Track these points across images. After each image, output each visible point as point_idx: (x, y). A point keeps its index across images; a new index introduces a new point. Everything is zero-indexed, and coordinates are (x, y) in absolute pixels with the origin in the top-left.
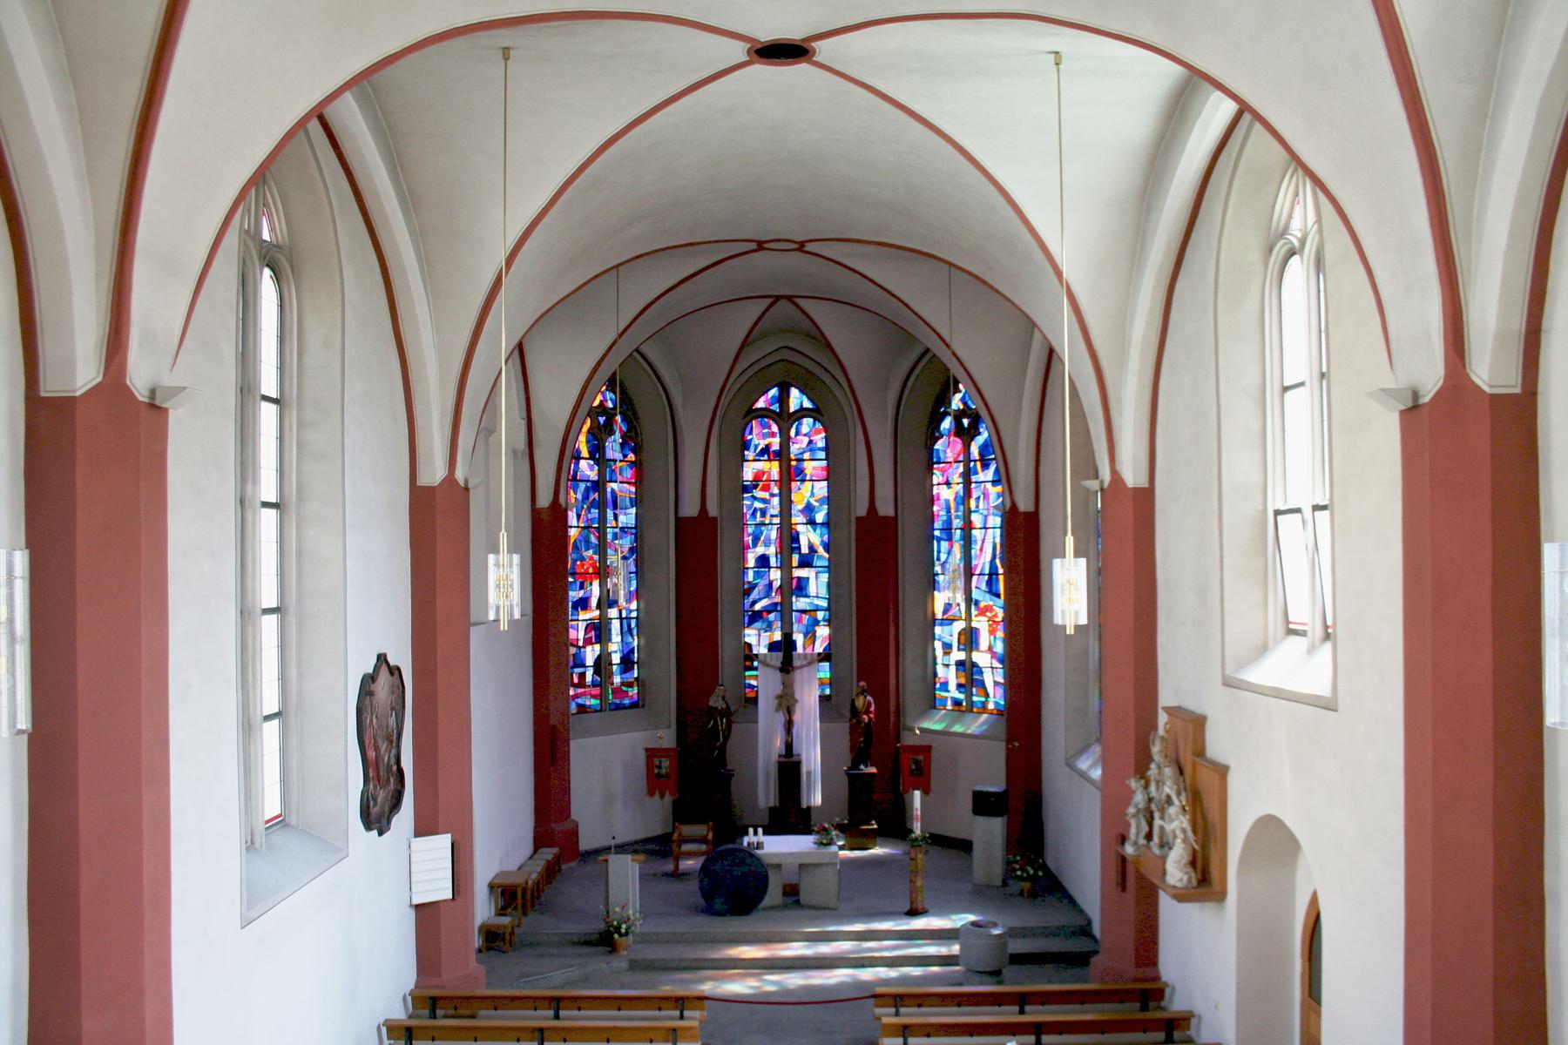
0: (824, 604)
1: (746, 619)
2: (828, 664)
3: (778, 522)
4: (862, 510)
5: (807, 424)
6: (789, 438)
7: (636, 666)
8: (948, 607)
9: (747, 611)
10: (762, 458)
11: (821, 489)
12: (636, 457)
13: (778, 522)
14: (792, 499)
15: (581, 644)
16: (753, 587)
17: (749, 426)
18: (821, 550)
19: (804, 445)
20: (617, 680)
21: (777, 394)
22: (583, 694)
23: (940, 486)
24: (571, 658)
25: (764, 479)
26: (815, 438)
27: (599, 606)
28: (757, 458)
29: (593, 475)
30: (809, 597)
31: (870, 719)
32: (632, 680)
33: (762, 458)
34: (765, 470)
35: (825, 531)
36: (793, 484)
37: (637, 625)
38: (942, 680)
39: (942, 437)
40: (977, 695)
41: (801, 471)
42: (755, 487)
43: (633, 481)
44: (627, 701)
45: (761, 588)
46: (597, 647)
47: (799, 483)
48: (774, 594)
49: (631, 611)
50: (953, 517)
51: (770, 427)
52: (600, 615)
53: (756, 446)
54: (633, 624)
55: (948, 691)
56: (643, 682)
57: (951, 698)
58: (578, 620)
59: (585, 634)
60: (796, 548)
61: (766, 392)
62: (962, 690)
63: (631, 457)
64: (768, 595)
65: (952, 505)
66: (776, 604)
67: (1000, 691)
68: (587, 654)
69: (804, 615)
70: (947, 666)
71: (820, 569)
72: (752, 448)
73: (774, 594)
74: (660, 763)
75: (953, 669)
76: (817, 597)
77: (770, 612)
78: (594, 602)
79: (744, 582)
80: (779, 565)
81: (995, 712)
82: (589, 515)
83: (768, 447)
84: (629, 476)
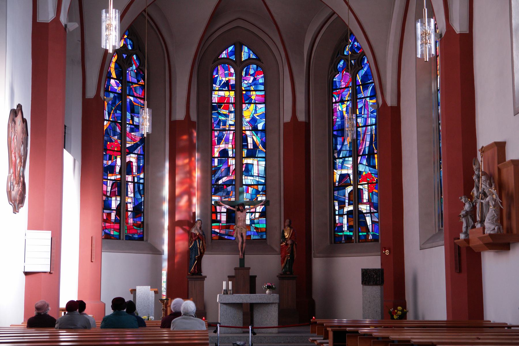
1: (213, 189)
2: (265, 219)
4: (287, 118)
6: (242, 76)
8: (342, 176)
9: (214, 185)
10: (224, 89)
11: (261, 108)
15: (109, 194)
16: (218, 169)
18: (261, 147)
19: (251, 81)
20: (131, 221)
21: (234, 50)
22: (110, 227)
28: (221, 89)
30: (253, 176)
33: (224, 89)
36: (244, 105)
38: (338, 225)
41: (249, 97)
42: (220, 107)
47: (247, 105)
53: (221, 81)
64: (227, 175)
69: (250, 188)
72: (218, 83)
78: (118, 169)
79: (212, 166)
80: (234, 156)
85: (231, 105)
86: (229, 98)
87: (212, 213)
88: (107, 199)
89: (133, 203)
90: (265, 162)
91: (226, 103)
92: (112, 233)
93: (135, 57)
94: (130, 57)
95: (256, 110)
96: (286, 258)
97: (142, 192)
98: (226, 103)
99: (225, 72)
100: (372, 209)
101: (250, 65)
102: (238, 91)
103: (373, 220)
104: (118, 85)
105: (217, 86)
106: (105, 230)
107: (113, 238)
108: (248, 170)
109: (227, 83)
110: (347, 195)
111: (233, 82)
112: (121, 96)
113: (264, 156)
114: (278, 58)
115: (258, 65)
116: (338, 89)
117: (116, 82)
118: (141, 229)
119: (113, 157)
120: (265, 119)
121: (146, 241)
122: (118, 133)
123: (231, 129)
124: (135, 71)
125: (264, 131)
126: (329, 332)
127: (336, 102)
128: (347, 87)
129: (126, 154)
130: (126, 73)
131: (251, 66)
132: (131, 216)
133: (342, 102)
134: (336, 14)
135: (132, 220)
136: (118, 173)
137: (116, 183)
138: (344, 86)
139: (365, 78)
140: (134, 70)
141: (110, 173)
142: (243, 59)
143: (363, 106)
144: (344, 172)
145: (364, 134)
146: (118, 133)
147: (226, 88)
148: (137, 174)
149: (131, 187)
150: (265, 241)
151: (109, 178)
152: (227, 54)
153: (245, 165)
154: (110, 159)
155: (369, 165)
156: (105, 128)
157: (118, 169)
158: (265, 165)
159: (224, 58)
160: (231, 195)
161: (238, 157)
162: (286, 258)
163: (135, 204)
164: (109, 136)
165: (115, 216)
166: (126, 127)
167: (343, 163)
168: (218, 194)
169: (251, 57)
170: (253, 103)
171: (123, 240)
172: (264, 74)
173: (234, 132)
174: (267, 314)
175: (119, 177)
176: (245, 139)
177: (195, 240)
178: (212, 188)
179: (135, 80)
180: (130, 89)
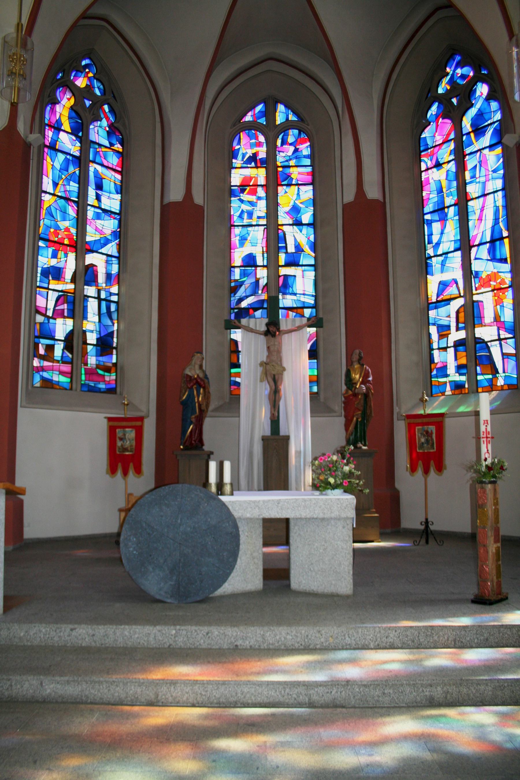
0: (311, 301)
2: (316, 361)
3: (265, 223)
4: (350, 196)
5: (292, 135)
6: (276, 146)
7: (114, 351)
8: (443, 286)
9: (234, 309)
10: (249, 166)
11: (307, 192)
12: (123, 149)
13: (265, 223)
14: (279, 202)
15: (50, 313)
16: (240, 285)
17: (237, 137)
18: (307, 249)
19: (290, 153)
20: (92, 361)
21: (264, 110)
22: (52, 369)
23: (430, 171)
24: (38, 326)
25: (251, 184)
26: (300, 147)
27: (73, 280)
28: (245, 165)
29: (75, 149)
30: (295, 294)
31: (368, 389)
32: (110, 365)
33: (249, 166)
34: (252, 176)
35: (311, 230)
36: (280, 188)
37: (117, 310)
38: (439, 366)
39: (429, 124)
40: (482, 374)
41: (288, 176)
42: (243, 191)
43: (120, 169)
44: (102, 386)
45: (247, 286)
46: (69, 323)
47: (285, 187)
48: (260, 292)
49: (111, 294)
50: (445, 195)
51: (257, 138)
52: (75, 289)
53: (244, 155)
54: (113, 307)
55: (447, 376)
56: (122, 368)
57: (450, 382)
58: (48, 288)
59: (56, 305)
60: (282, 247)
61: (254, 108)
62: (464, 371)
63: (118, 147)
64: (254, 293)
65: (444, 184)
66: (262, 301)
67: (511, 364)
68: (57, 326)
69: (290, 313)
70: (445, 349)
71: (306, 268)
72: (240, 157)
73: (260, 292)
74: (124, 435)
75: (451, 351)
76: (304, 294)
77: (256, 309)
78: (68, 274)
79: (231, 280)
80: (265, 264)
81: (506, 387)
82: (68, 187)
83: (255, 155)
84: (115, 164)
86: (256, 178)
87: (232, 352)
88: (47, 322)
89: (96, 331)
90: (314, 273)
93: (106, 107)
95: (298, 194)
96: (355, 419)
97: (115, 316)
98: (252, 186)
99: (251, 141)
100: (501, 332)
101: (289, 129)
102: (271, 167)
103: (504, 352)
105: (238, 162)
106: (41, 373)
107: (58, 387)
109: (254, 158)
110: (453, 315)
113: (313, 262)
115: (301, 129)
116: (431, 148)
118: (112, 374)
120: (314, 207)
122: (71, 218)
123: (260, 223)
124: (105, 129)
125: (312, 226)
126: (70, 278)
127: (427, 169)
128: (446, 141)
129: (84, 251)
131: (291, 132)
132: (94, 352)
133: (438, 165)
134: (290, 548)
136: (69, 281)
137: (65, 296)
138: (441, 142)
140: (105, 127)
141: (53, 279)
142: (278, 122)
143: (476, 166)
144: (447, 277)
145: (482, 210)
148: (106, 286)
149: (92, 305)
150: (316, 395)
151: (51, 287)
152: (254, 115)
153: (282, 277)
158: (315, 276)
162: (355, 419)
163: (100, 334)
165: (63, 350)
167: (443, 264)
170: (294, 185)
171: (76, 390)
172: (309, 141)
173: (265, 228)
174: (324, 545)
177: (191, 388)
178: (231, 314)
180: (96, 153)
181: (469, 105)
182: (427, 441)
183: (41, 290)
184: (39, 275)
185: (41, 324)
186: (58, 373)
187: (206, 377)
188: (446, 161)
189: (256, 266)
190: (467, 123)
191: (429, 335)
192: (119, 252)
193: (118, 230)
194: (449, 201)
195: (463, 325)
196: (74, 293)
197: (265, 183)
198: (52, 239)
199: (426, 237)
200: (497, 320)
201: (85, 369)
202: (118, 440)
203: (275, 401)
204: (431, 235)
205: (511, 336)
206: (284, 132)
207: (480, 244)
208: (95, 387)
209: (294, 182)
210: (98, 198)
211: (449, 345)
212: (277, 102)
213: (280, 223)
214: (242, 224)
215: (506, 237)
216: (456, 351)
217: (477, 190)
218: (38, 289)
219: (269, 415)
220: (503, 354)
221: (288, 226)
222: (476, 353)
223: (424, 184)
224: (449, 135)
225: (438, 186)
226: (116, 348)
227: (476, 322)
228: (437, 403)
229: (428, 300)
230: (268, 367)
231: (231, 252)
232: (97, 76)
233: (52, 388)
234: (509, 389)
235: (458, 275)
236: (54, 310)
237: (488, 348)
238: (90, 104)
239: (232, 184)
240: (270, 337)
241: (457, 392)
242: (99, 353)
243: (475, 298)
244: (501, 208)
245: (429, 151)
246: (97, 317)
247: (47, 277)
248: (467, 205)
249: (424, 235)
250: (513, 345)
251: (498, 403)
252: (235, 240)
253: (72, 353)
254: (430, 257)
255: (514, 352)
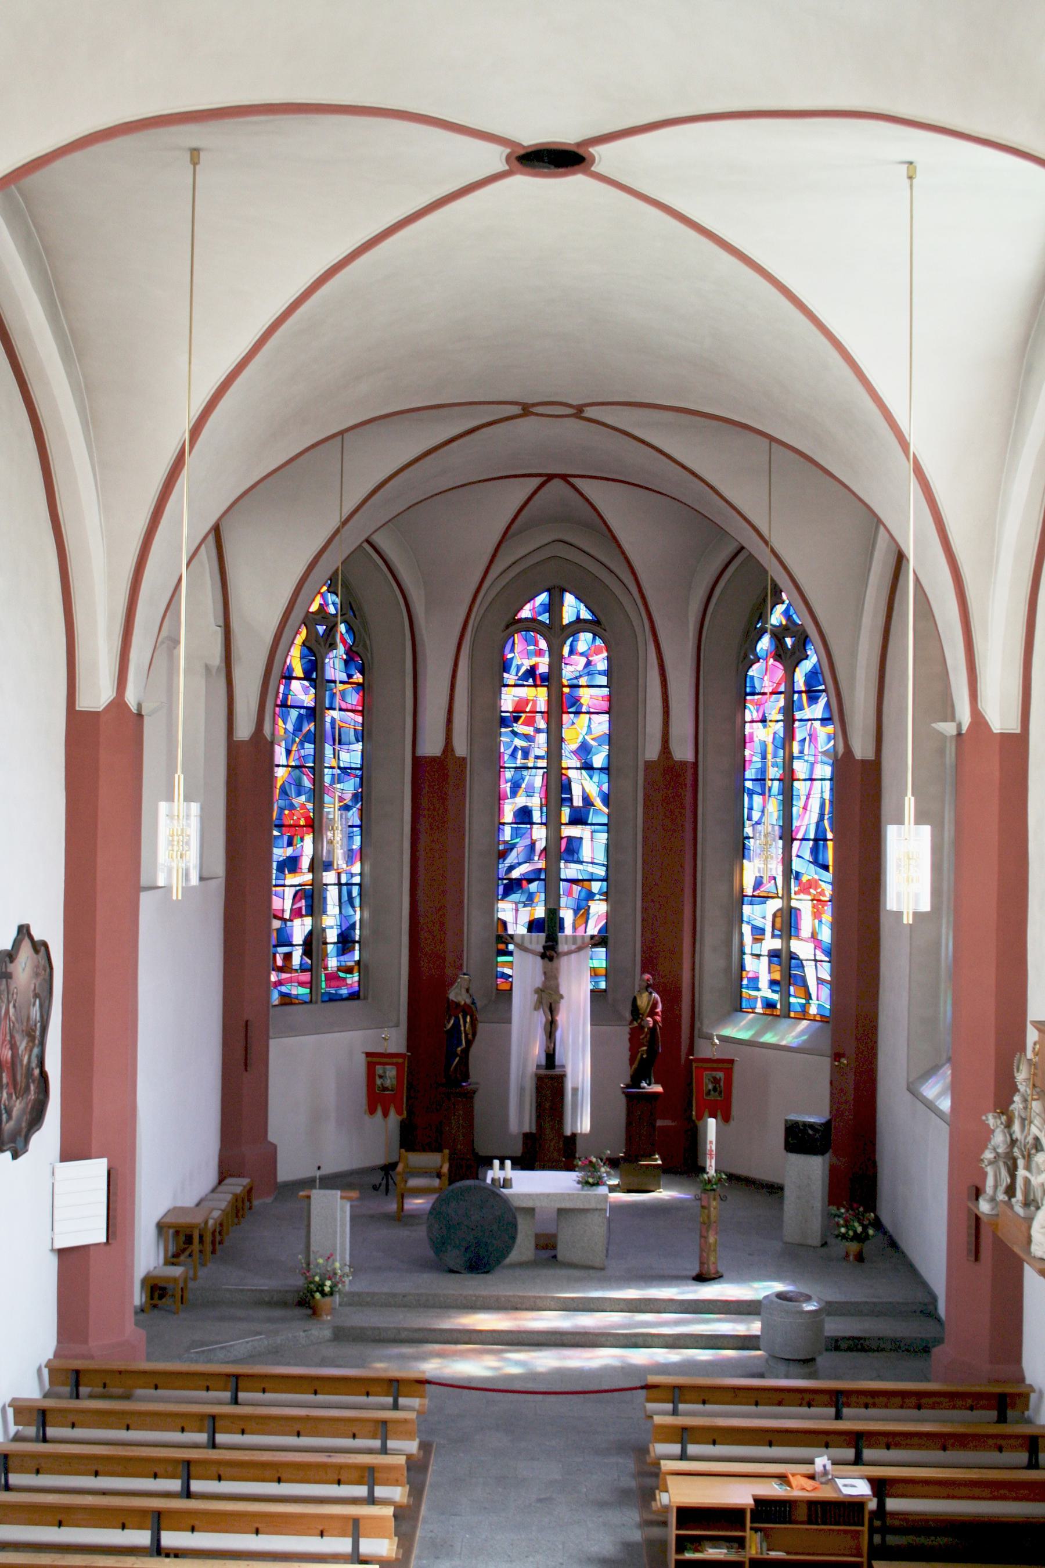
0: (601, 872)
2: (604, 949)
3: (545, 765)
4: (652, 752)
5: (584, 641)
6: (562, 657)
7: (357, 946)
10: (525, 683)
11: (601, 724)
13: (545, 765)
15: (287, 916)
16: (511, 847)
17: (511, 641)
18: (598, 803)
19: (580, 667)
20: (332, 963)
21: (547, 601)
22: (290, 981)
24: (275, 934)
26: (594, 658)
27: (312, 869)
28: (520, 682)
30: (581, 862)
33: (525, 683)
35: (605, 778)
36: (565, 716)
37: (360, 894)
38: (750, 975)
39: (758, 661)
40: (795, 996)
41: (576, 701)
42: (516, 719)
45: (520, 849)
46: (308, 921)
47: (572, 716)
48: (536, 858)
49: (352, 875)
51: (536, 644)
52: (313, 879)
53: (519, 668)
54: (355, 891)
55: (758, 989)
56: (367, 967)
57: (762, 997)
59: (293, 904)
62: (777, 988)
63: (358, 678)
64: (529, 860)
65: (770, 748)
66: (540, 870)
67: (825, 992)
69: (574, 886)
70: (758, 956)
72: (513, 670)
73: (536, 858)
74: (385, 1072)
75: (765, 960)
76: (592, 863)
77: (530, 881)
78: (305, 863)
80: (544, 821)
85: (538, 716)
86: (535, 702)
91: (529, 712)
92: (294, 992)
93: (342, 628)
94: (332, 629)
98: (529, 712)
99: (529, 648)
104: (306, 692)
105: (511, 677)
106: (279, 988)
107: (297, 1001)
108: (571, 850)
109: (532, 672)
110: (770, 918)
111: (543, 669)
112: (313, 713)
113: (606, 821)
114: (638, 630)
117: (303, 686)
119: (297, 839)
121: (364, 999)
122: (307, 789)
123: (539, 765)
125: (606, 771)
130: (323, 664)
132: (334, 953)
135: (335, 959)
136: (307, 871)
139: (812, 677)
142: (565, 621)
143: (805, 739)
146: (307, 789)
147: (531, 680)
151: (287, 882)
153: (565, 839)
154: (290, 844)
155: (815, 862)
156: (279, 784)
157: (305, 863)
159: (526, 619)
160: (536, 900)
161: (552, 823)
164: (287, 797)
165: (301, 957)
166: (322, 775)
168: (510, 898)
169: (582, 617)
170: (585, 713)
173: (544, 773)
175: (308, 877)
176: (566, 787)
179: (344, 677)
181: (804, 657)
182: (715, 1089)
183: (277, 888)
184: (274, 871)
185: (278, 930)
186: (296, 984)
187: (473, 1003)
188: (774, 719)
189: (532, 823)
190: (800, 682)
191: (741, 934)
192: (361, 821)
193: (360, 790)
194: (774, 772)
195: (779, 933)
196: (311, 885)
197: (546, 710)
198: (286, 823)
199: (746, 811)
200: (814, 936)
201: (326, 974)
202: (377, 1078)
203: (551, 1033)
204: (751, 809)
205: (827, 959)
206: (573, 635)
207: (803, 839)
208: (336, 994)
209: (584, 710)
210: (336, 755)
211: (762, 953)
212: (563, 590)
213: (564, 765)
214: (514, 765)
215: (831, 840)
216: (770, 962)
217: (804, 771)
218: (274, 889)
219: (544, 1047)
220: (818, 978)
221: (575, 771)
222: (790, 970)
223: (747, 740)
224: (779, 684)
225: (763, 748)
226: (358, 942)
227: (793, 934)
228: (744, 1022)
229: (742, 892)
230: (544, 995)
231: (500, 804)
232: (331, 590)
233: (292, 1004)
234: (821, 1021)
235: (776, 869)
236: (292, 910)
237: (803, 966)
238: (325, 630)
239: (503, 709)
240: (546, 960)
241: (768, 1011)
242: (341, 952)
243: (794, 904)
244: (827, 803)
245: (756, 697)
246: (338, 908)
247: (283, 872)
248: (792, 786)
249: (743, 807)
250: (829, 970)
251: (805, 1038)
252: (506, 787)
253: (311, 958)
254: (748, 838)
255: (829, 978)
